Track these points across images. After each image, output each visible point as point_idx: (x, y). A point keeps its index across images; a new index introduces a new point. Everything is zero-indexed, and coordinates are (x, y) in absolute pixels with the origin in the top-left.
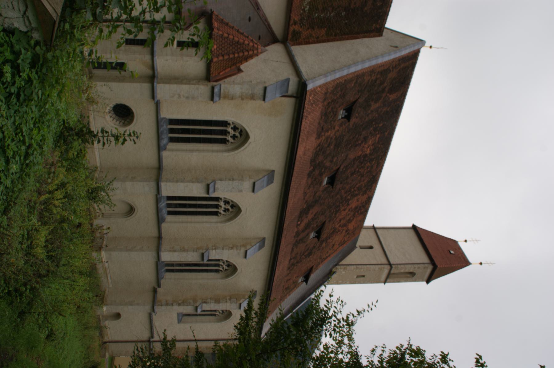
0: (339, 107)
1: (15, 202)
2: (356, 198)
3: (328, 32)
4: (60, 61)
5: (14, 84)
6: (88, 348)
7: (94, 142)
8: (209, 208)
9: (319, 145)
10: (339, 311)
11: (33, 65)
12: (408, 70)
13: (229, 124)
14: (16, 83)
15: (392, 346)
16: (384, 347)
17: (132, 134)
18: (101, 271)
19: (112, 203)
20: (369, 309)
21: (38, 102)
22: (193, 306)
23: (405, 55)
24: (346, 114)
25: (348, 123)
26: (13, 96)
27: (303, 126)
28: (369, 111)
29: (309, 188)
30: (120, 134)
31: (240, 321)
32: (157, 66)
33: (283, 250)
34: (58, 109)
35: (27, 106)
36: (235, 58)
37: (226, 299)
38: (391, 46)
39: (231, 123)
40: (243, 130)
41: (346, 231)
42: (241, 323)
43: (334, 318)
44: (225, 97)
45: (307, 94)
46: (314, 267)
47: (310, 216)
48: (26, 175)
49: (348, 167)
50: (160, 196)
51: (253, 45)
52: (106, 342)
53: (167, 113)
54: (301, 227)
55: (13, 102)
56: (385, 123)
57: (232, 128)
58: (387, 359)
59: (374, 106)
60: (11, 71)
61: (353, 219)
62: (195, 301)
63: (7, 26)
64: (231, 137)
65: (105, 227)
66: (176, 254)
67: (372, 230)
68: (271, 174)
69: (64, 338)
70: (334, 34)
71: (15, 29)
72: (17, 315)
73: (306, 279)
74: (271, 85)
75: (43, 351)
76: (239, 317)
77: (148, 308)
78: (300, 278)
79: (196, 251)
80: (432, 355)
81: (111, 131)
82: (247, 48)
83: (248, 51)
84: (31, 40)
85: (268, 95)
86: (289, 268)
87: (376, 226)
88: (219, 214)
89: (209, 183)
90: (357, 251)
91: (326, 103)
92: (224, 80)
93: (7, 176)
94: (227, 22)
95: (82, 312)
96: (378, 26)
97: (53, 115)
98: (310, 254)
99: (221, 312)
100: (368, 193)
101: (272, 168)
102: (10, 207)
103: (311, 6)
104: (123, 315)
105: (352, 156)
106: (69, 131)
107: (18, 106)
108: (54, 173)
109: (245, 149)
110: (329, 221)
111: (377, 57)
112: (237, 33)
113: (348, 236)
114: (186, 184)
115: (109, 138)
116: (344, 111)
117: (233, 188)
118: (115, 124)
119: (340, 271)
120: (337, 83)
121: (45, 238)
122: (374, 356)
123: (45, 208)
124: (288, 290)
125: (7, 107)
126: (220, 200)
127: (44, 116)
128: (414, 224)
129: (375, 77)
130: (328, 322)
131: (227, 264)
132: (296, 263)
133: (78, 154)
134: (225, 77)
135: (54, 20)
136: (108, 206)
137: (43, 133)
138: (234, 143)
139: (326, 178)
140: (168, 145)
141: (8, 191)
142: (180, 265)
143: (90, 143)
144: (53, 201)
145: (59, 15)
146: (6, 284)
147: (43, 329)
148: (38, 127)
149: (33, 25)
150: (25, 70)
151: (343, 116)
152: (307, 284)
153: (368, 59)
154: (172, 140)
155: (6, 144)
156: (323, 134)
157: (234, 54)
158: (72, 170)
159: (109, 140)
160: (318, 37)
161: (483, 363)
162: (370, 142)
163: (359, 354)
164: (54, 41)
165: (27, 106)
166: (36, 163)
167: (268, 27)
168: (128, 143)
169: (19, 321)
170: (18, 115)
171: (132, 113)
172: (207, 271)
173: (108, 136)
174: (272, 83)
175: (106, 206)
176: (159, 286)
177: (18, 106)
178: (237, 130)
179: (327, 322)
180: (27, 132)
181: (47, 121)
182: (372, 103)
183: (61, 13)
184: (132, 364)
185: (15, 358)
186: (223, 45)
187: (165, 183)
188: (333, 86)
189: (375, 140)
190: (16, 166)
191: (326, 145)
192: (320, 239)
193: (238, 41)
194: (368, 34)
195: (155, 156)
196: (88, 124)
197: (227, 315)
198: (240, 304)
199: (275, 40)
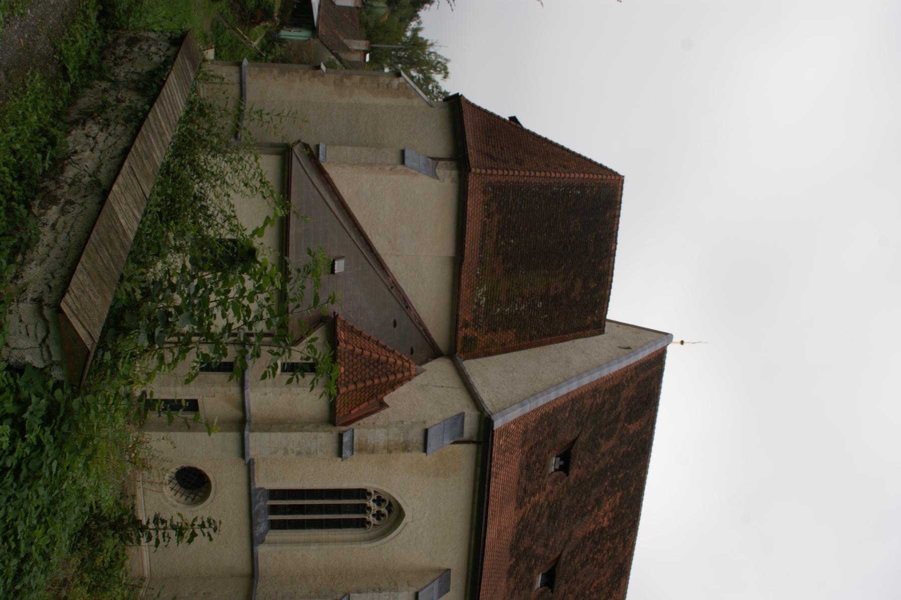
0: (549, 453)
3: (519, 335)
4: (92, 411)
5: (12, 452)
7: (142, 539)
11: (47, 420)
12: (653, 383)
13: (370, 494)
14: (17, 450)
17: (207, 525)
21: (49, 480)
24: (562, 463)
25: (566, 478)
26: (9, 472)
27: (492, 489)
30: (187, 524)
32: (249, 407)
34: (84, 488)
35: (29, 488)
36: (374, 386)
38: (620, 348)
39: (373, 493)
44: (361, 450)
49: (575, 553)
53: (264, 481)
56: (628, 471)
57: (374, 501)
64: (373, 515)
68: (445, 576)
70: (528, 337)
74: (435, 425)
81: (171, 520)
82: (392, 370)
84: (49, 380)
91: (526, 449)
92: (358, 422)
94: (360, 330)
96: (595, 319)
100: (615, 595)
101: (446, 565)
103: (489, 298)
105: (579, 533)
106: (99, 522)
111: (599, 367)
112: (376, 346)
115: (167, 531)
118: (178, 502)
127: (58, 502)
129: (601, 398)
133: (112, 561)
134: (360, 418)
135: (88, 350)
137: (53, 532)
139: (540, 576)
140: (268, 534)
143: (134, 541)
145: (97, 341)
148: (46, 521)
149: (54, 359)
150: (33, 429)
151: (557, 467)
153: (586, 371)
154: (275, 525)
156: (526, 500)
158: (98, 588)
159: (166, 535)
160: (504, 344)
165: (29, 488)
166: (34, 588)
167: (424, 334)
168: (201, 540)
170: (12, 504)
171: (208, 481)
173: (165, 528)
174: (436, 422)
177: (15, 490)
182: (602, 442)
183: (100, 338)
186: (355, 367)
188: (535, 419)
189: (615, 501)
191: (534, 519)
194: (582, 332)
196: (133, 508)
199: (435, 353)
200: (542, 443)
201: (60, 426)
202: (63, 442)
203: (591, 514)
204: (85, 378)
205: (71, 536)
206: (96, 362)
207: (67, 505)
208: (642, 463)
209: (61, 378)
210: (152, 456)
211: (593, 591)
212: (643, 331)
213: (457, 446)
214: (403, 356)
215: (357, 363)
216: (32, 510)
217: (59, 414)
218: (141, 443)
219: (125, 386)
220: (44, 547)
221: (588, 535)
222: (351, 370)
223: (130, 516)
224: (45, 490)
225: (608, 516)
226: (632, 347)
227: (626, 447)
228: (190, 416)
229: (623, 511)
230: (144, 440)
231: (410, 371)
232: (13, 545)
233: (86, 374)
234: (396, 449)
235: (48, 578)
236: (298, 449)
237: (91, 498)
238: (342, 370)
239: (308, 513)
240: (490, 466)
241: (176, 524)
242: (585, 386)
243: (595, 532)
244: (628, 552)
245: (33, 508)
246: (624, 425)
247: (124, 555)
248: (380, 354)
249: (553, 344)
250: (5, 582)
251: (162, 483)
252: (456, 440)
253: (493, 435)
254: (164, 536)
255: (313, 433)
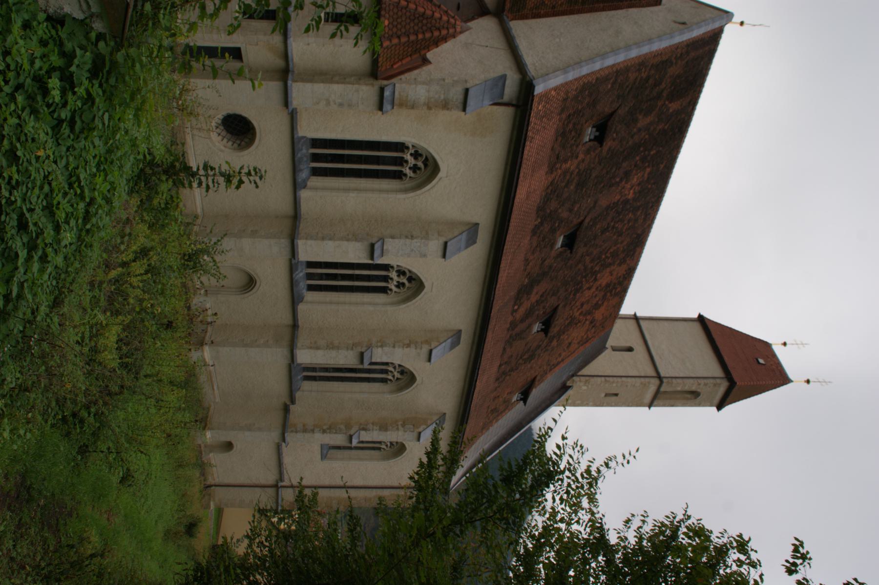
0: (586, 123)
1: (71, 288)
2: (608, 270)
4: (138, 66)
5: (65, 105)
6: (183, 495)
7: (193, 184)
8: (373, 280)
9: (552, 183)
10: (577, 462)
11: (94, 73)
12: (702, 63)
13: (408, 148)
14: (69, 103)
15: (659, 514)
16: (646, 515)
17: (253, 173)
18: (203, 378)
19: (220, 274)
20: (625, 462)
21: (103, 131)
22: (346, 433)
23: (697, 36)
24: (597, 134)
25: (600, 149)
26: (65, 124)
27: (526, 152)
28: (635, 130)
29: (533, 253)
30: (234, 172)
31: (419, 469)
32: (292, 55)
33: (489, 351)
34: (136, 138)
35: (86, 139)
37: (397, 425)
38: (675, 22)
39: (411, 147)
40: (430, 160)
41: (591, 322)
42: (420, 472)
43: (567, 473)
44: (401, 105)
45: (534, 101)
46: (538, 378)
47: (534, 298)
48: (86, 246)
50: (296, 262)
51: (449, 20)
52: (210, 486)
53: (309, 129)
54: (518, 316)
55: (64, 134)
56: (661, 149)
57: (411, 155)
58: (649, 535)
59: (643, 121)
60: (60, 86)
61: (603, 303)
62: (348, 426)
63: (52, 11)
64: (410, 168)
65: (210, 312)
66: (320, 353)
67: (633, 322)
68: (473, 229)
69: (147, 481)
71: (66, 15)
72: (77, 450)
73: (525, 397)
74: (477, 85)
75: (115, 501)
76: (417, 463)
77: (275, 435)
78: (515, 394)
79: (352, 349)
80: (722, 531)
81: (220, 168)
82: (437, 25)
83: (439, 29)
84: (91, 32)
85: (471, 102)
86: (497, 379)
87: (638, 315)
88: (389, 291)
89: (373, 242)
90: (607, 354)
91: (564, 116)
92: (399, 77)
93: (58, 250)
95: (174, 444)
97: (127, 149)
98: (531, 357)
99: (389, 444)
101: (475, 220)
102: (63, 295)
104: (237, 446)
105: (604, 202)
107: (73, 140)
108: (130, 234)
109: (432, 188)
110: (565, 306)
111: (650, 41)
113: (593, 330)
114: (337, 243)
115: (215, 178)
116: (594, 129)
117: (412, 250)
118: (225, 147)
119: (579, 386)
120: (584, 83)
121: (116, 336)
122: (629, 530)
123: (117, 289)
124: (496, 413)
125: (55, 143)
126: (390, 269)
128: (701, 314)
129: (646, 73)
130: (559, 479)
131: (399, 370)
132: (509, 371)
133: (167, 203)
136: (215, 278)
137: (112, 179)
138: (415, 178)
139: (562, 238)
140: (310, 180)
141: (60, 272)
142: (326, 370)
144: (129, 279)
146: (59, 406)
147: (116, 469)
148: (104, 170)
149: (93, 10)
150: (82, 82)
151: (592, 137)
152: (525, 405)
153: (636, 44)
154: (316, 172)
155: (55, 202)
156: (558, 166)
157: (417, 35)
159: (215, 181)
160: (554, 7)
161: (805, 553)
162: (635, 180)
163: (606, 527)
164: (128, 32)
165: (86, 139)
166: (102, 227)
168: (247, 186)
169: (79, 459)
171: (253, 128)
172: (368, 380)
173: (214, 175)
174: (478, 82)
175: (212, 278)
176: (293, 401)
177: (73, 140)
178: (419, 158)
179: (556, 478)
180: (86, 181)
181: (118, 159)
182: (640, 117)
184: (250, 534)
185: (75, 513)
186: (399, 20)
187: (304, 241)
188: (577, 88)
189: (643, 176)
190: (71, 234)
191: (564, 184)
192: (549, 335)
193: (424, 13)
195: (289, 198)
196: (183, 155)
197: (399, 449)
198: (420, 433)
199: (483, 12)
200: (580, 111)
201: (107, 79)
202: (112, 94)
203: (619, 185)
204: (127, 30)
205: (128, 181)
206: (137, 12)
207: (122, 154)
208: (676, 142)
209: (103, 31)
210: (199, 103)
211: (609, 255)
212: (703, 6)
213: (495, 107)
214: (449, 11)
215: (401, 16)
216: (90, 160)
217: (105, 67)
218: (188, 90)
219: (167, 38)
220: (106, 192)
221: (612, 205)
222: (395, 23)
223: (181, 162)
224: (100, 140)
225: (635, 189)
226: (687, 22)
227: (663, 125)
228: (235, 65)
229: (650, 186)
230: (190, 87)
231: (455, 28)
232: (79, 191)
233: (128, 24)
234: (436, 107)
235: (113, 219)
236: (340, 101)
237: (143, 148)
238: (386, 23)
239: (348, 162)
240: (527, 130)
241: (224, 171)
242: (633, 58)
243: (620, 203)
244: (647, 224)
245: (91, 158)
246: (665, 104)
247: (178, 198)
248: (426, 8)
249: (606, 10)
250: (77, 222)
251: (209, 130)
252: (496, 101)
253: (533, 100)
254: (213, 182)
255: (355, 86)
